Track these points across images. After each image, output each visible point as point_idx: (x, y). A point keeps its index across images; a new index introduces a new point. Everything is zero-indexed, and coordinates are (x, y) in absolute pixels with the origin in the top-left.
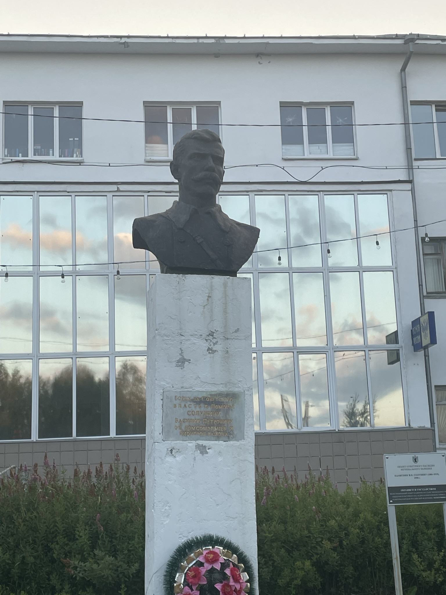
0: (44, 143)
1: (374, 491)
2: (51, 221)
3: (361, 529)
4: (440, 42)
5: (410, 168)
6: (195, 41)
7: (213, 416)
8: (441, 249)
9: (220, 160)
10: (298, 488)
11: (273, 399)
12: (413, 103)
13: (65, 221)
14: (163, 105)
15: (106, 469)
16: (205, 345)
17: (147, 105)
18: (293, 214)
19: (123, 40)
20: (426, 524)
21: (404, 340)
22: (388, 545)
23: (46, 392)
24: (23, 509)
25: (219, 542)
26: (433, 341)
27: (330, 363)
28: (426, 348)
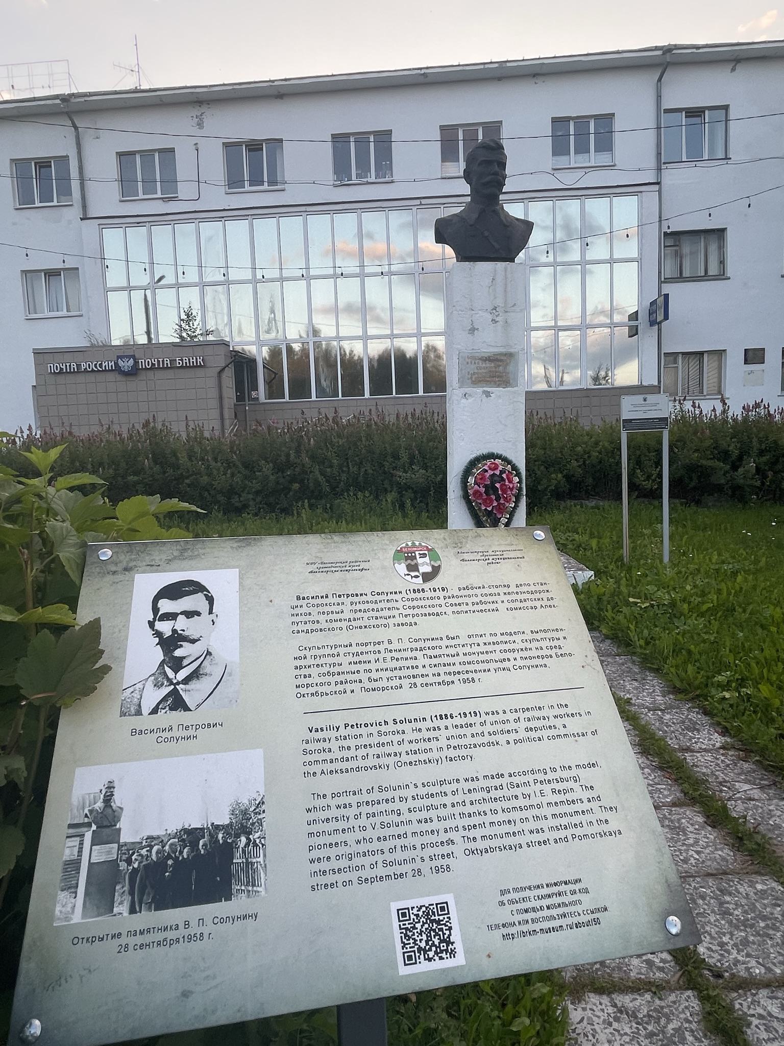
0: (363, 167)
1: (611, 427)
2: (370, 236)
3: (600, 453)
4: (694, 50)
5: (659, 169)
6: (482, 67)
7: (495, 370)
8: (679, 241)
9: (503, 165)
10: (555, 425)
11: (538, 369)
12: (667, 111)
13: (381, 235)
14: (455, 128)
15: (418, 412)
16: (490, 317)
17: (443, 128)
18: (559, 221)
19: (423, 72)
20: (648, 449)
21: (643, 318)
22: (619, 463)
23: (373, 366)
24: (363, 439)
25: (499, 457)
26: (666, 317)
27: (583, 338)
28: (660, 323)
